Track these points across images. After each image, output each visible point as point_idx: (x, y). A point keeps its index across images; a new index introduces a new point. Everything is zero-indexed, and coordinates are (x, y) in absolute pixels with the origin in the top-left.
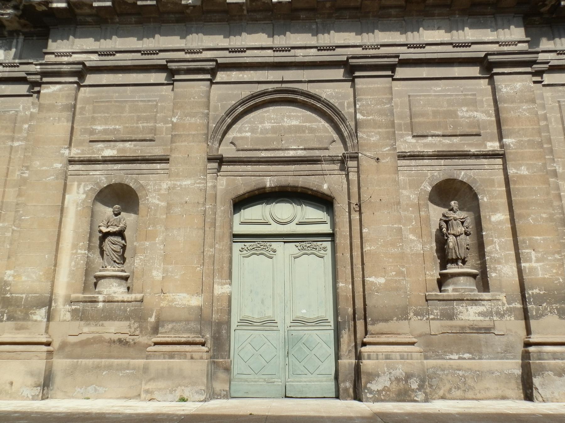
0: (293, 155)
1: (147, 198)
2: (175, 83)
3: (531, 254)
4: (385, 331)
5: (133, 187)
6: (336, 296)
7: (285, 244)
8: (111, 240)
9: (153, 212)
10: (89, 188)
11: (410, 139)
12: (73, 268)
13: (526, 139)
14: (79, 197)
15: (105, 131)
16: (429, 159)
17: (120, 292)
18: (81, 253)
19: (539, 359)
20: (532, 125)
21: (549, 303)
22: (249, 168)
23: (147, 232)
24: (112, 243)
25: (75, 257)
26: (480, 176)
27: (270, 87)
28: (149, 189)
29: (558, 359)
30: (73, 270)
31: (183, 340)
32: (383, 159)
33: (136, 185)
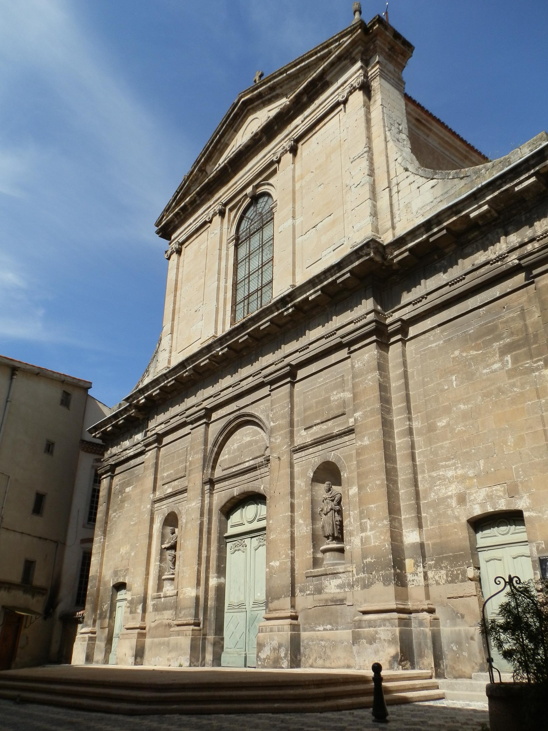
0: (252, 464)
2: (536, 280)
3: (367, 524)
4: (277, 607)
11: (303, 433)
13: (368, 409)
15: (168, 476)
16: (312, 447)
19: (359, 628)
20: (374, 393)
21: (378, 571)
22: (227, 483)
26: (344, 453)
27: (231, 417)
29: (372, 627)
31: (185, 622)
32: (283, 457)
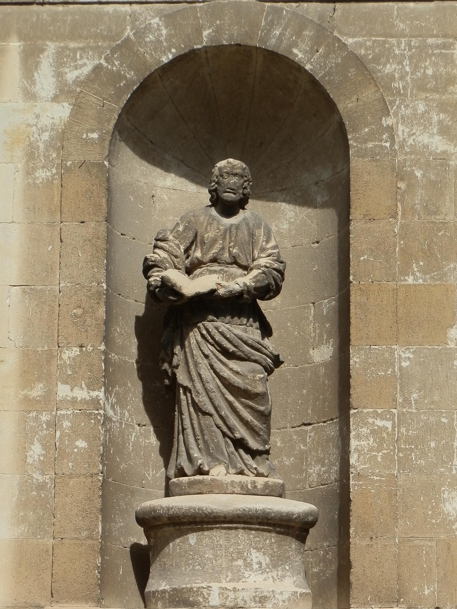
1: (388, 121)
5: (308, 67)
6: (202, 522)
7: (132, 5)
8: (218, 337)
9: (420, 192)
10: (86, 70)
12: (38, 477)
14: (38, 116)
17: (286, 596)
18: (74, 401)
23: (401, 295)
24: (225, 352)
25: (45, 417)
28: (392, 78)
30: (42, 487)
33: (326, 56)
